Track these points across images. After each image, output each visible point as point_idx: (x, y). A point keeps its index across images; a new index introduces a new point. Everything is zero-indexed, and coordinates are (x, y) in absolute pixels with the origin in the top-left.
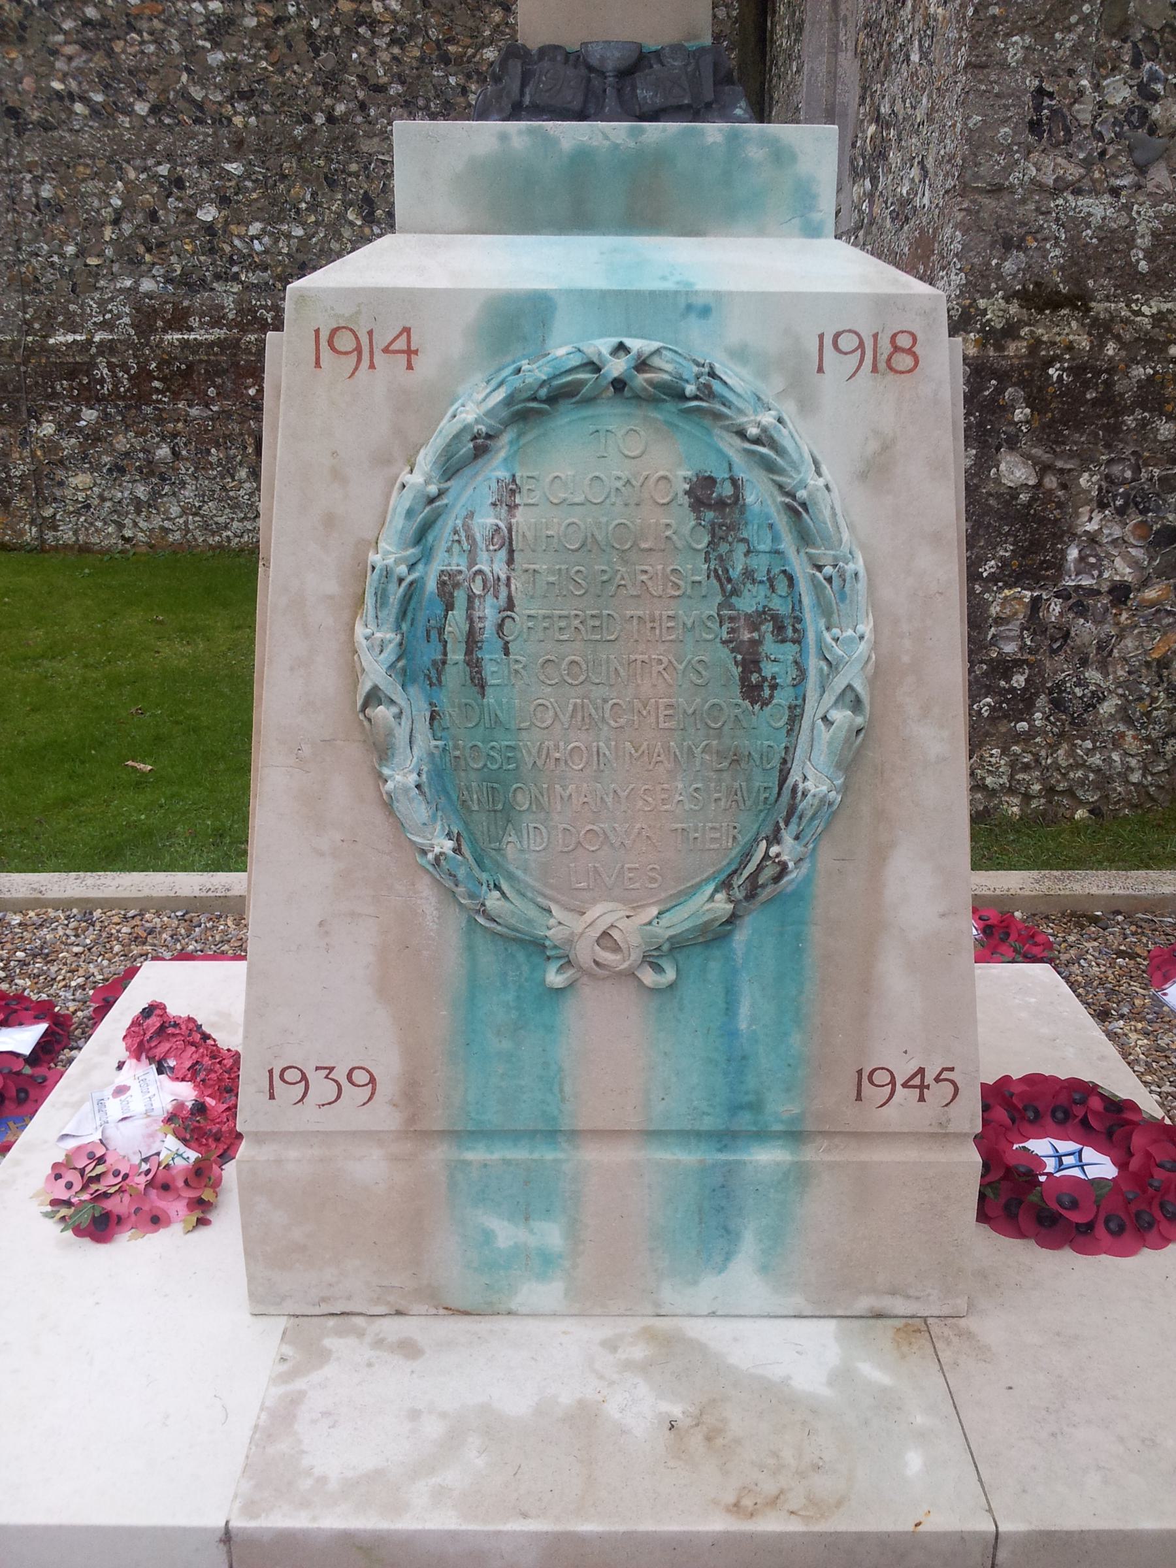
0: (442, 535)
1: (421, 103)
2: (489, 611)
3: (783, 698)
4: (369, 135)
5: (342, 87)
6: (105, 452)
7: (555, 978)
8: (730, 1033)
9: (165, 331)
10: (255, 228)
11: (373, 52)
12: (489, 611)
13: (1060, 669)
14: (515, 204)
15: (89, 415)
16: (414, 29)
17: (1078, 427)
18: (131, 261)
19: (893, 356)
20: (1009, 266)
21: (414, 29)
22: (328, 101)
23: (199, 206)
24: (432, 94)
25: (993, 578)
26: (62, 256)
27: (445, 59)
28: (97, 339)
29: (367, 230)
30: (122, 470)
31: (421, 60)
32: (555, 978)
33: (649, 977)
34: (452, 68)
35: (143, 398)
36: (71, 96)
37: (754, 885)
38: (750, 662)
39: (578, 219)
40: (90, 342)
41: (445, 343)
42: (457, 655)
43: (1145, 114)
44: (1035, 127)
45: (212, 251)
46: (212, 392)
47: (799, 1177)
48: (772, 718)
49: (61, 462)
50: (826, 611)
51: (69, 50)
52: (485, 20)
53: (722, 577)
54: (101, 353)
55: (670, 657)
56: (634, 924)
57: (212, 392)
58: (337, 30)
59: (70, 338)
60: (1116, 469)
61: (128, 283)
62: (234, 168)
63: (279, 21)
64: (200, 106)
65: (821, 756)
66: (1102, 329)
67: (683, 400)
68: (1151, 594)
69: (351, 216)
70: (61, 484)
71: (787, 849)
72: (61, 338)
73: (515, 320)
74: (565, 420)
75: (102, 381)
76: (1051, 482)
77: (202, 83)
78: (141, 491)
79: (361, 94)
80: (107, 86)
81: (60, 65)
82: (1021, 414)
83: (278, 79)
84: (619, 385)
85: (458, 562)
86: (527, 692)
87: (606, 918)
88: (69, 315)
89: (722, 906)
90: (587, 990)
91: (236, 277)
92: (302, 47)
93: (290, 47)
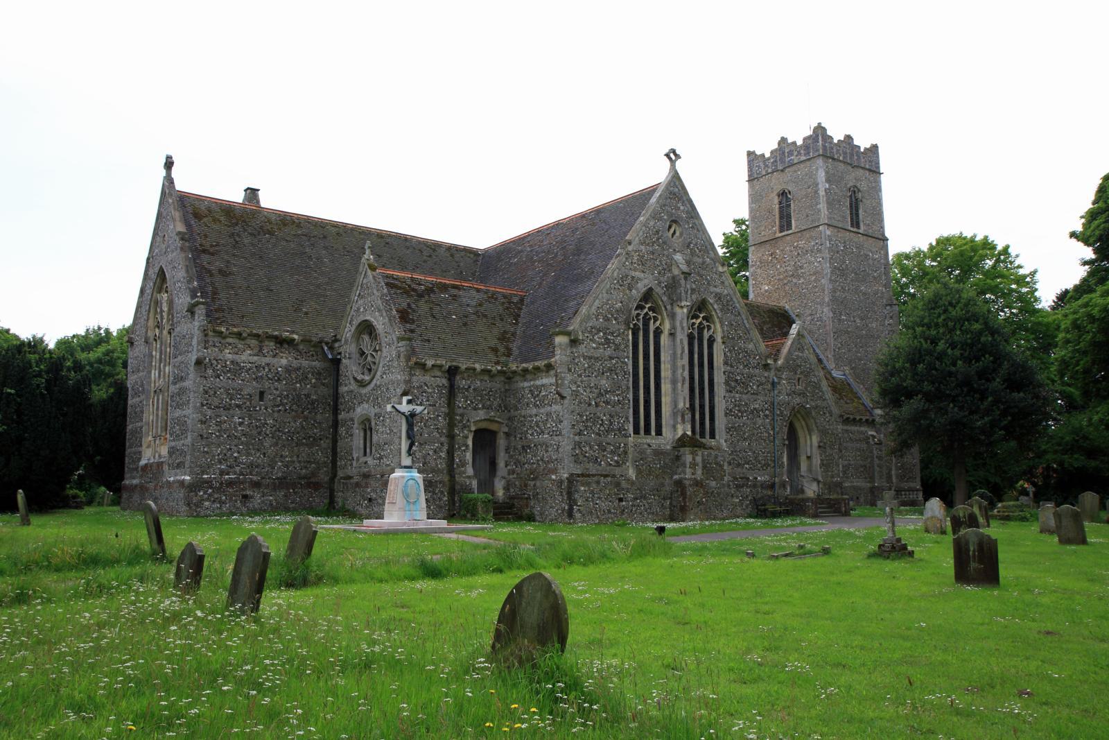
15: (210, 491)
72: (206, 476)
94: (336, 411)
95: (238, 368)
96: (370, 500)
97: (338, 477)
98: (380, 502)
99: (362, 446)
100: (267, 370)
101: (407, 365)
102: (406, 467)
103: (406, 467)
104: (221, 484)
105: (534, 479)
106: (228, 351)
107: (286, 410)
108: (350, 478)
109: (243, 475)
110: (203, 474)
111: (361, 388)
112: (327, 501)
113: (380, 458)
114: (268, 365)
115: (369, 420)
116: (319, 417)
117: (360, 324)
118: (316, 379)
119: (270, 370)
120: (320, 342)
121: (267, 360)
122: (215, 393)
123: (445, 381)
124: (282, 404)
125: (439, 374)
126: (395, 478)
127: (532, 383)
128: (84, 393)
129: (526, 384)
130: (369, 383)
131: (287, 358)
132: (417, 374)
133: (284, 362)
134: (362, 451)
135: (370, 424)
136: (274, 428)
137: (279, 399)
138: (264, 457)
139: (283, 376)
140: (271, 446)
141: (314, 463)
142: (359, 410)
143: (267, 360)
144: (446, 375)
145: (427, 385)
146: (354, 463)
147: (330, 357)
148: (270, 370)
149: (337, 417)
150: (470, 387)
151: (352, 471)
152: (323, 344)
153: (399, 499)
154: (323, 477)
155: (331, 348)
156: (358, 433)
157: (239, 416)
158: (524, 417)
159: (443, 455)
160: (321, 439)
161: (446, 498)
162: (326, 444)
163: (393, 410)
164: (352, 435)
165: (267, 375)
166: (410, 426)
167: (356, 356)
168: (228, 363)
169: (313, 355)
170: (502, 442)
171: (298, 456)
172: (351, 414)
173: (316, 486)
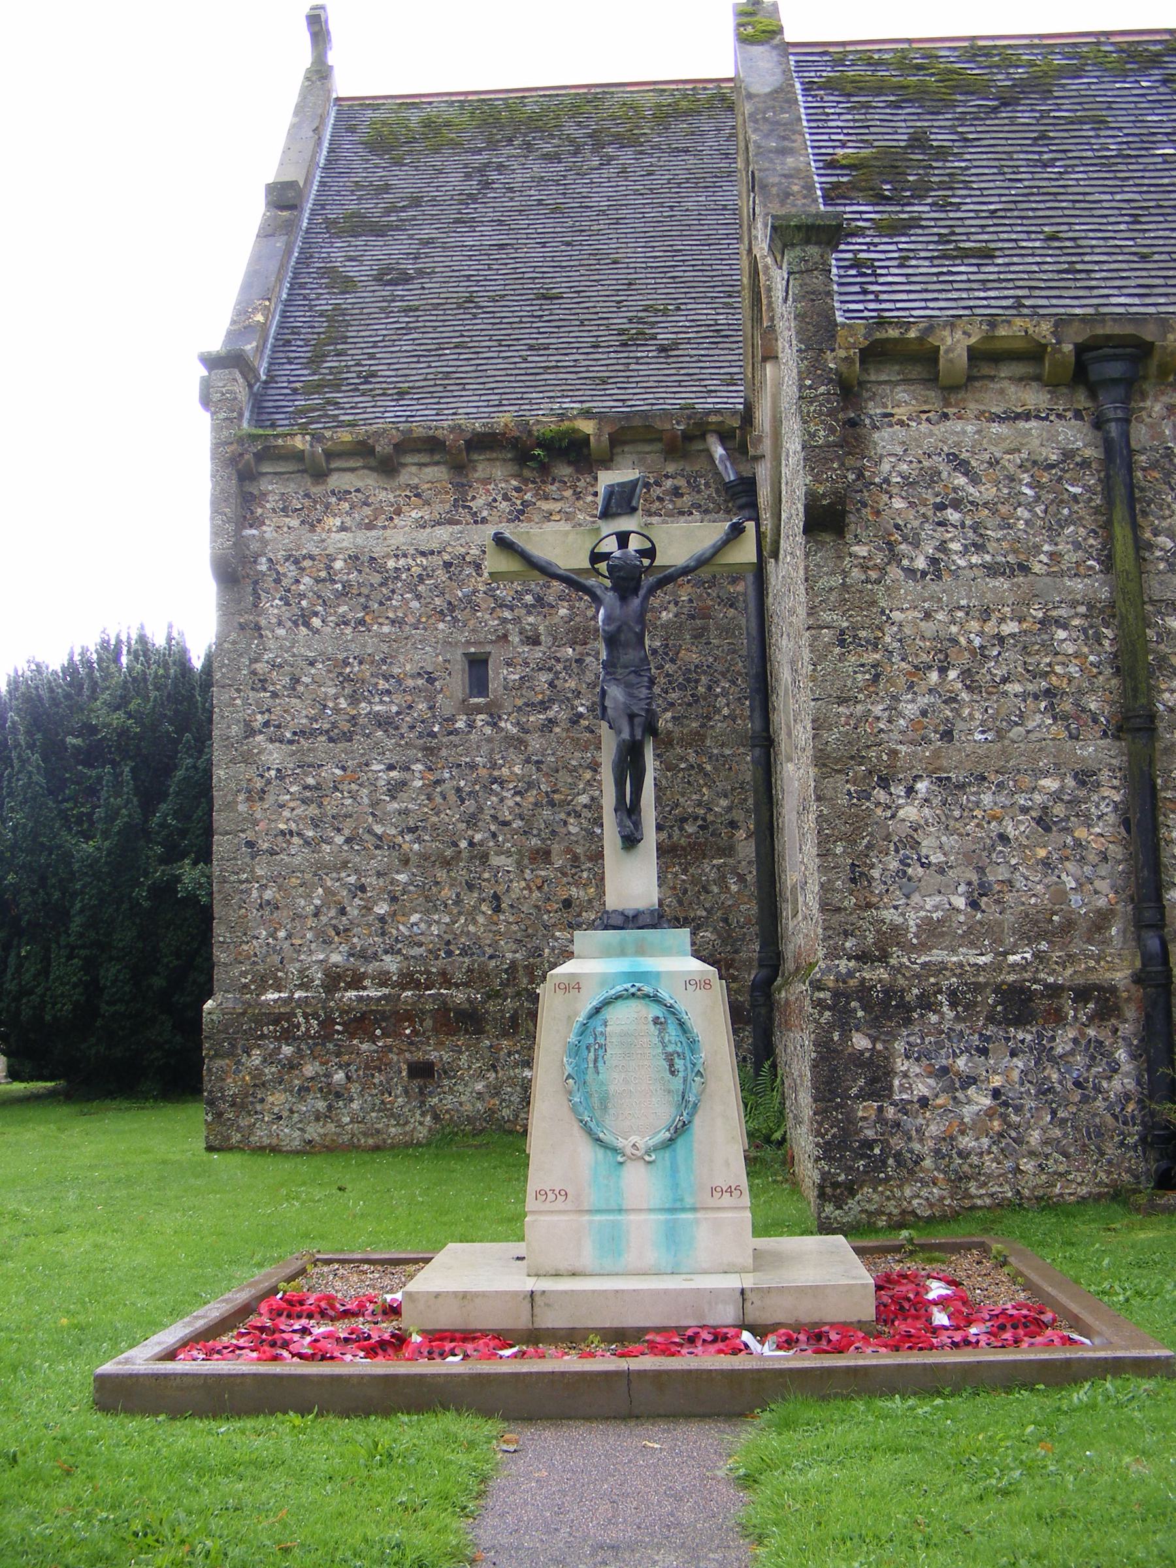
3: (681, 1074)
4: (498, 854)
6: (297, 1077)
9: (346, 990)
10: (415, 918)
11: (502, 800)
13: (897, 1143)
14: (607, 952)
15: (287, 1050)
16: (530, 785)
17: (890, 1019)
18: (324, 942)
19: (706, 984)
20: (848, 945)
22: (470, 832)
23: (376, 903)
24: (543, 826)
25: (857, 1097)
26: (276, 939)
27: (552, 804)
28: (296, 996)
30: (308, 1089)
31: (536, 804)
32: (620, 1159)
33: (647, 1158)
34: (557, 809)
35: (328, 1037)
36: (291, 833)
38: (671, 1065)
40: (291, 998)
43: (905, 872)
44: (853, 880)
45: (383, 934)
46: (378, 1032)
49: (263, 1084)
51: (292, 804)
52: (579, 778)
53: (662, 1042)
54: (300, 1007)
57: (378, 1032)
58: (477, 787)
59: (276, 996)
60: (912, 1039)
61: (321, 957)
62: (402, 878)
63: (438, 782)
64: (380, 838)
66: (898, 970)
68: (939, 1101)
69: (484, 908)
70: (262, 1101)
72: (271, 996)
75: (298, 1026)
76: (879, 1046)
77: (380, 821)
78: (321, 1105)
80: (317, 826)
81: (286, 813)
82: (860, 1014)
83: (435, 819)
84: (633, 994)
88: (276, 978)
89: (668, 1135)
90: (629, 1164)
91: (399, 952)
92: (452, 798)
93: (444, 798)
95: (376, 579)
102: (631, 921)
103: (631, 921)
104: (327, 1023)
106: (338, 522)
107: (576, 719)
109: (417, 985)
110: (263, 989)
122: (296, 680)
124: (556, 694)
125: (1034, 397)
132: (901, 413)
137: (544, 677)
145: (962, 466)
157: (390, 757)
168: (338, 565)
169: (676, 492)
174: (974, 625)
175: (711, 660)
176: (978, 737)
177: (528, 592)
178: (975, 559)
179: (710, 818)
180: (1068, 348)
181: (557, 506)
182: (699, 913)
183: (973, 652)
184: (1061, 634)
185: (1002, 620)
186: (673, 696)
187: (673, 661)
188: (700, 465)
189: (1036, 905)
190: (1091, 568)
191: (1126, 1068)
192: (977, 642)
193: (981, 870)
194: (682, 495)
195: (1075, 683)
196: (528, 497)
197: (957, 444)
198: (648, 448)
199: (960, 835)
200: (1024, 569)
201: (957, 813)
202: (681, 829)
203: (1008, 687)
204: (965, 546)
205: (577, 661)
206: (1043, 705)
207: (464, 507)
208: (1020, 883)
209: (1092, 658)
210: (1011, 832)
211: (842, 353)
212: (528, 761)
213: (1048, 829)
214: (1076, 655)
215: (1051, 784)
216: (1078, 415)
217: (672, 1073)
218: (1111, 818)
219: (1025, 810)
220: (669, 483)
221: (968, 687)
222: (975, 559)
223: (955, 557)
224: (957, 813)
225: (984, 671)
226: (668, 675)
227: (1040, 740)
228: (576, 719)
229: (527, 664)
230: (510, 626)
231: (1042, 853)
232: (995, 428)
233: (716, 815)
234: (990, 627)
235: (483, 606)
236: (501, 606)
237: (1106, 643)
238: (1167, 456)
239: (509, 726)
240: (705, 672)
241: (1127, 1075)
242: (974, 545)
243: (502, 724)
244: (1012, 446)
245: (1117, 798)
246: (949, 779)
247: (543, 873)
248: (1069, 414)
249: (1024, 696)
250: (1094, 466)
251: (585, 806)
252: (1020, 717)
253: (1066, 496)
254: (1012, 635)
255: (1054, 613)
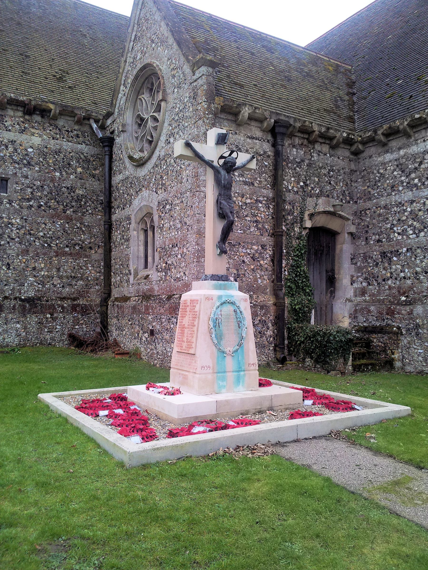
0: (216, 314)
1: (24, 243)
2: (220, 321)
3: (241, 328)
4: (9, 249)
5: (3, 238)
7: (225, 355)
8: (238, 360)
11: (12, 231)
12: (220, 321)
16: (23, 227)
19: (246, 300)
21: (23, 227)
27: (30, 234)
29: (8, 271)
31: (24, 234)
32: (225, 355)
33: (232, 355)
37: (240, 345)
38: (239, 325)
39: (220, 289)
41: (215, 299)
42: (217, 325)
47: (245, 375)
48: (241, 330)
50: (243, 321)
55: (233, 325)
56: (232, 349)
58: (3, 225)
65: (244, 333)
67: (233, 303)
69: (4, 267)
71: (242, 342)
73: (220, 297)
74: (224, 305)
79: (8, 240)
85: (217, 317)
86: (223, 328)
87: (229, 349)
94: (108, 208)
96: (152, 333)
97: (112, 298)
98: (167, 337)
99: (142, 254)
100: (11, 149)
101: (209, 107)
102: (215, 277)
105: (407, 303)
107: (40, 206)
108: (126, 299)
111: (139, 170)
112: (98, 330)
113: (167, 269)
114: (13, 142)
115: (150, 215)
116: (87, 219)
117: (136, 77)
118: (83, 168)
119: (16, 150)
120: (88, 118)
121: (11, 136)
123: (267, 147)
125: (258, 134)
126: (47, 408)
127: (402, 152)
128: (274, 338)
129: (388, 157)
130: (149, 158)
131: (40, 136)
133: (36, 140)
134: (143, 261)
135: (152, 221)
136: (22, 231)
137: (29, 190)
138: (9, 269)
139: (35, 159)
140: (18, 255)
141: (82, 279)
142: (136, 203)
143: (11, 136)
144: (270, 137)
146: (131, 278)
147: (100, 135)
148: (16, 150)
149: (110, 218)
150: (303, 161)
151: (129, 290)
152: (92, 122)
153: (204, 349)
154: (94, 297)
155: (103, 128)
156: (135, 235)
158: (385, 207)
159: (266, 262)
160: (91, 248)
161: (269, 333)
162: (97, 255)
163: (188, 153)
164: (128, 240)
165: (11, 157)
166: (224, 189)
167: (132, 127)
170: (345, 248)
171: (58, 270)
172: (128, 211)
173: (85, 311)
174: (240, 198)
175: (86, 194)
176: (239, 231)
177: (25, 159)
178: (241, 179)
179: (84, 245)
180: (273, 121)
181: (37, 131)
182: (79, 275)
183: (239, 206)
184: (260, 205)
185: (247, 198)
186: (74, 204)
187: (74, 192)
188: (86, 128)
189: (250, 281)
190: (268, 187)
191: (271, 328)
192: (240, 204)
193: (237, 270)
194: (79, 137)
195: (263, 219)
196: (26, 125)
197: (239, 143)
198: (69, 119)
199: (233, 259)
200: (253, 184)
201: (233, 253)
202: (74, 247)
203: (247, 218)
204: (239, 174)
205: (41, 186)
206: (255, 225)
207: (2, 124)
208: (247, 275)
209: (267, 213)
210: (246, 260)
211: (216, 106)
212: (22, 218)
213: (254, 260)
214: (264, 212)
215: (255, 247)
216: (268, 141)
217: (239, 327)
218: (269, 259)
219: (249, 254)
220: (75, 132)
221: (237, 217)
222: (241, 179)
223: (236, 177)
224: (233, 253)
225: (241, 212)
226: (72, 197)
227: (253, 235)
228: (40, 206)
229: (23, 184)
230: (17, 170)
231: (252, 267)
232: (248, 140)
233: (85, 244)
234: (244, 200)
235: (8, 161)
236: (15, 162)
237: (271, 209)
238: (288, 158)
239: (16, 205)
240: (84, 198)
241: (271, 330)
242: (241, 174)
243: (13, 204)
244: (252, 147)
245: (270, 254)
246: (231, 243)
247: (26, 258)
248: (266, 141)
249: (251, 221)
250: (271, 157)
251: (42, 236)
252: (250, 227)
253: (264, 165)
254: (249, 203)
255: (259, 199)
